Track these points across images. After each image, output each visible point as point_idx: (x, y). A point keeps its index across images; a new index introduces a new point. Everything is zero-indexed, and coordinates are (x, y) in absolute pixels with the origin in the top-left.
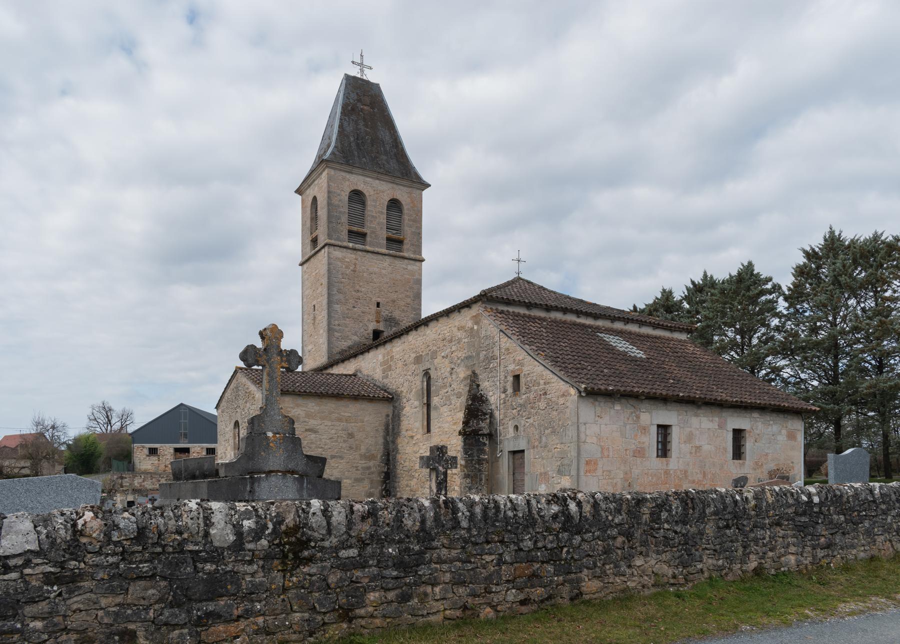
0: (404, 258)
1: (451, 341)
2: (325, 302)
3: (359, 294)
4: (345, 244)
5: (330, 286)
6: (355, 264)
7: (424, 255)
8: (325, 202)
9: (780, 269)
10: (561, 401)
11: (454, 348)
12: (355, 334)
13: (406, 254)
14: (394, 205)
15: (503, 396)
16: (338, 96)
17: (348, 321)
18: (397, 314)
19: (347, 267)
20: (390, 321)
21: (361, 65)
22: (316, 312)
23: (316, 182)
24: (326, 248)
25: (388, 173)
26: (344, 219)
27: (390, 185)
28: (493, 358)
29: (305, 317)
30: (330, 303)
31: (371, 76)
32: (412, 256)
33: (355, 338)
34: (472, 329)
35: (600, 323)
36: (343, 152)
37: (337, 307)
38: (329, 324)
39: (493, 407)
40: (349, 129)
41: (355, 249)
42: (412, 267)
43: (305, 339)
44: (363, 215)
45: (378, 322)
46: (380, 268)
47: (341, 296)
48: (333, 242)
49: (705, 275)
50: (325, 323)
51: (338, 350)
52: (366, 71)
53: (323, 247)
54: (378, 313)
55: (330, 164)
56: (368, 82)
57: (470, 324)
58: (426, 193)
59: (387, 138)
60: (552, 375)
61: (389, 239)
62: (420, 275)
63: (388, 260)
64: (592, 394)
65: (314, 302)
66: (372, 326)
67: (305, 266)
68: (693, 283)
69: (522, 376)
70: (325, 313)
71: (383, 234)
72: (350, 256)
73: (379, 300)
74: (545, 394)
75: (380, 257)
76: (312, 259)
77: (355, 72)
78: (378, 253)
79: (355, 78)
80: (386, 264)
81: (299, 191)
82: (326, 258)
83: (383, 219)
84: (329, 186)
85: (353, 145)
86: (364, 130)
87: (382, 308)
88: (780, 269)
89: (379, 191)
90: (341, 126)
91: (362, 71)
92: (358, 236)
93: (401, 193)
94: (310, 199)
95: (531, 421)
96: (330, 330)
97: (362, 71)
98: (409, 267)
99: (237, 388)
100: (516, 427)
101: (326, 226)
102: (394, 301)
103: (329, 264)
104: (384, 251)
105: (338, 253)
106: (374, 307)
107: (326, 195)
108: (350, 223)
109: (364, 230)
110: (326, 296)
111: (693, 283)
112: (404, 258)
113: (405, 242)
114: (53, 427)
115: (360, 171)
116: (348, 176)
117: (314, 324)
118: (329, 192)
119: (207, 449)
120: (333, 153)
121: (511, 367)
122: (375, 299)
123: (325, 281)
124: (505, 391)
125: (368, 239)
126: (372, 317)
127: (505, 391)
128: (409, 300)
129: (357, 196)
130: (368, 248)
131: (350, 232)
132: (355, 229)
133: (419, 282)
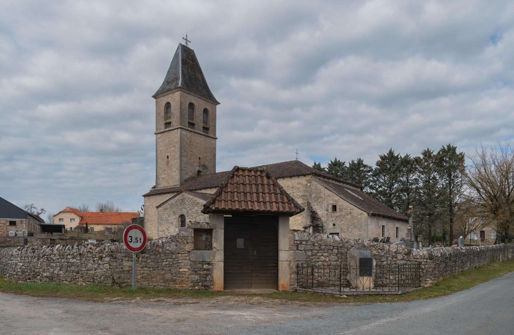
0: (209, 137)
1: (293, 188)
2: (178, 155)
3: (193, 153)
4: (187, 128)
5: (181, 148)
6: (191, 138)
7: (217, 136)
8: (178, 107)
9: (371, 161)
10: (359, 216)
11: (295, 191)
12: (191, 172)
13: (210, 135)
14: (206, 111)
15: (326, 212)
16: (176, 55)
17: (188, 166)
18: (207, 164)
19: (188, 140)
20: (205, 167)
21: (186, 39)
22: (169, 159)
23: (170, 95)
24: (179, 130)
25: (204, 96)
26: (187, 116)
27: (204, 102)
28: (320, 197)
29: (159, 161)
30: (181, 156)
31: (190, 46)
32: (213, 136)
33: (191, 174)
34: (306, 185)
35: (345, 185)
36: (185, 84)
37: (184, 158)
38: (181, 166)
39: (320, 216)
40: (186, 72)
41: (191, 131)
42: (212, 141)
43: (160, 171)
44: (193, 115)
45: (199, 167)
46: (200, 140)
47: (185, 154)
48: (182, 127)
49: (336, 159)
50: (178, 165)
51: (184, 179)
52: (188, 43)
53: (177, 129)
54: (200, 162)
55: (182, 89)
56: (189, 48)
57: (305, 183)
58: (218, 107)
59: (200, 78)
60: (354, 207)
61: (204, 128)
62: (216, 145)
63: (203, 137)
64: (374, 215)
65: (168, 154)
66: (197, 169)
67: (159, 135)
68: (331, 162)
69: (337, 206)
70: (178, 161)
71: (202, 125)
72: (189, 134)
73: (200, 156)
74: (351, 213)
75: (201, 136)
76: (166, 133)
77: (184, 43)
78: (200, 134)
79: (184, 46)
80: (203, 139)
81: (155, 97)
82: (179, 134)
83: (201, 117)
84: (181, 100)
85: (188, 80)
86: (188, 75)
87: (201, 160)
88: (371, 161)
89: (200, 104)
90: (182, 70)
91: (187, 43)
92: (191, 125)
93: (208, 106)
94: (164, 103)
95: (343, 222)
96: (181, 170)
97: (187, 43)
98: (212, 142)
99: (183, 200)
100: (334, 225)
101: (179, 119)
102: (206, 157)
103: (181, 137)
104: (202, 133)
105: (184, 133)
106: (198, 160)
107: (179, 104)
108: (189, 119)
109: (194, 122)
110: (179, 153)
111: (331, 162)
112: (209, 137)
113: (210, 129)
114: (101, 210)
115: (193, 94)
116: (188, 95)
117: (167, 165)
118: (181, 103)
119: (10, 222)
120: (182, 84)
121: (331, 202)
122: (199, 156)
123: (178, 145)
124: (327, 210)
125: (196, 126)
126: (197, 164)
127: (327, 210)
128: (211, 157)
129: (191, 105)
130: (196, 131)
131: (189, 122)
132: (191, 121)
133: (215, 149)
